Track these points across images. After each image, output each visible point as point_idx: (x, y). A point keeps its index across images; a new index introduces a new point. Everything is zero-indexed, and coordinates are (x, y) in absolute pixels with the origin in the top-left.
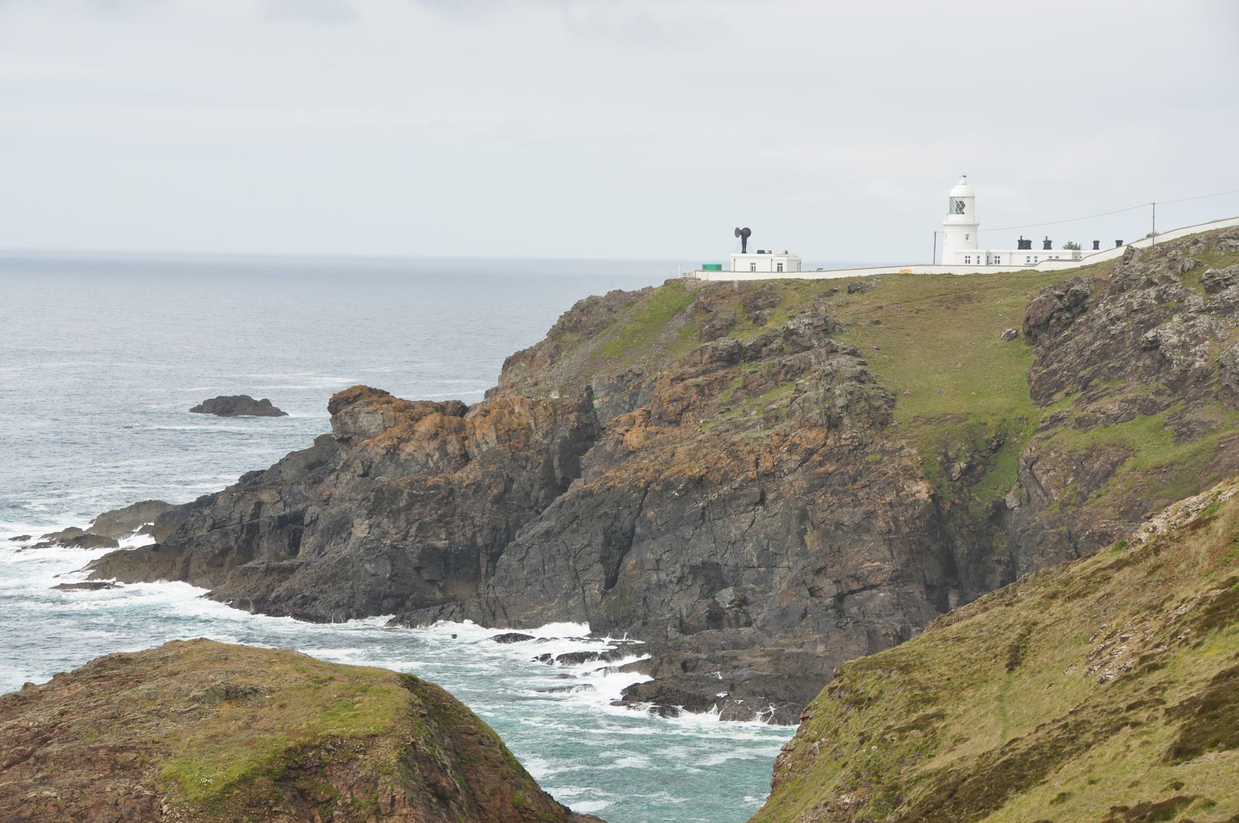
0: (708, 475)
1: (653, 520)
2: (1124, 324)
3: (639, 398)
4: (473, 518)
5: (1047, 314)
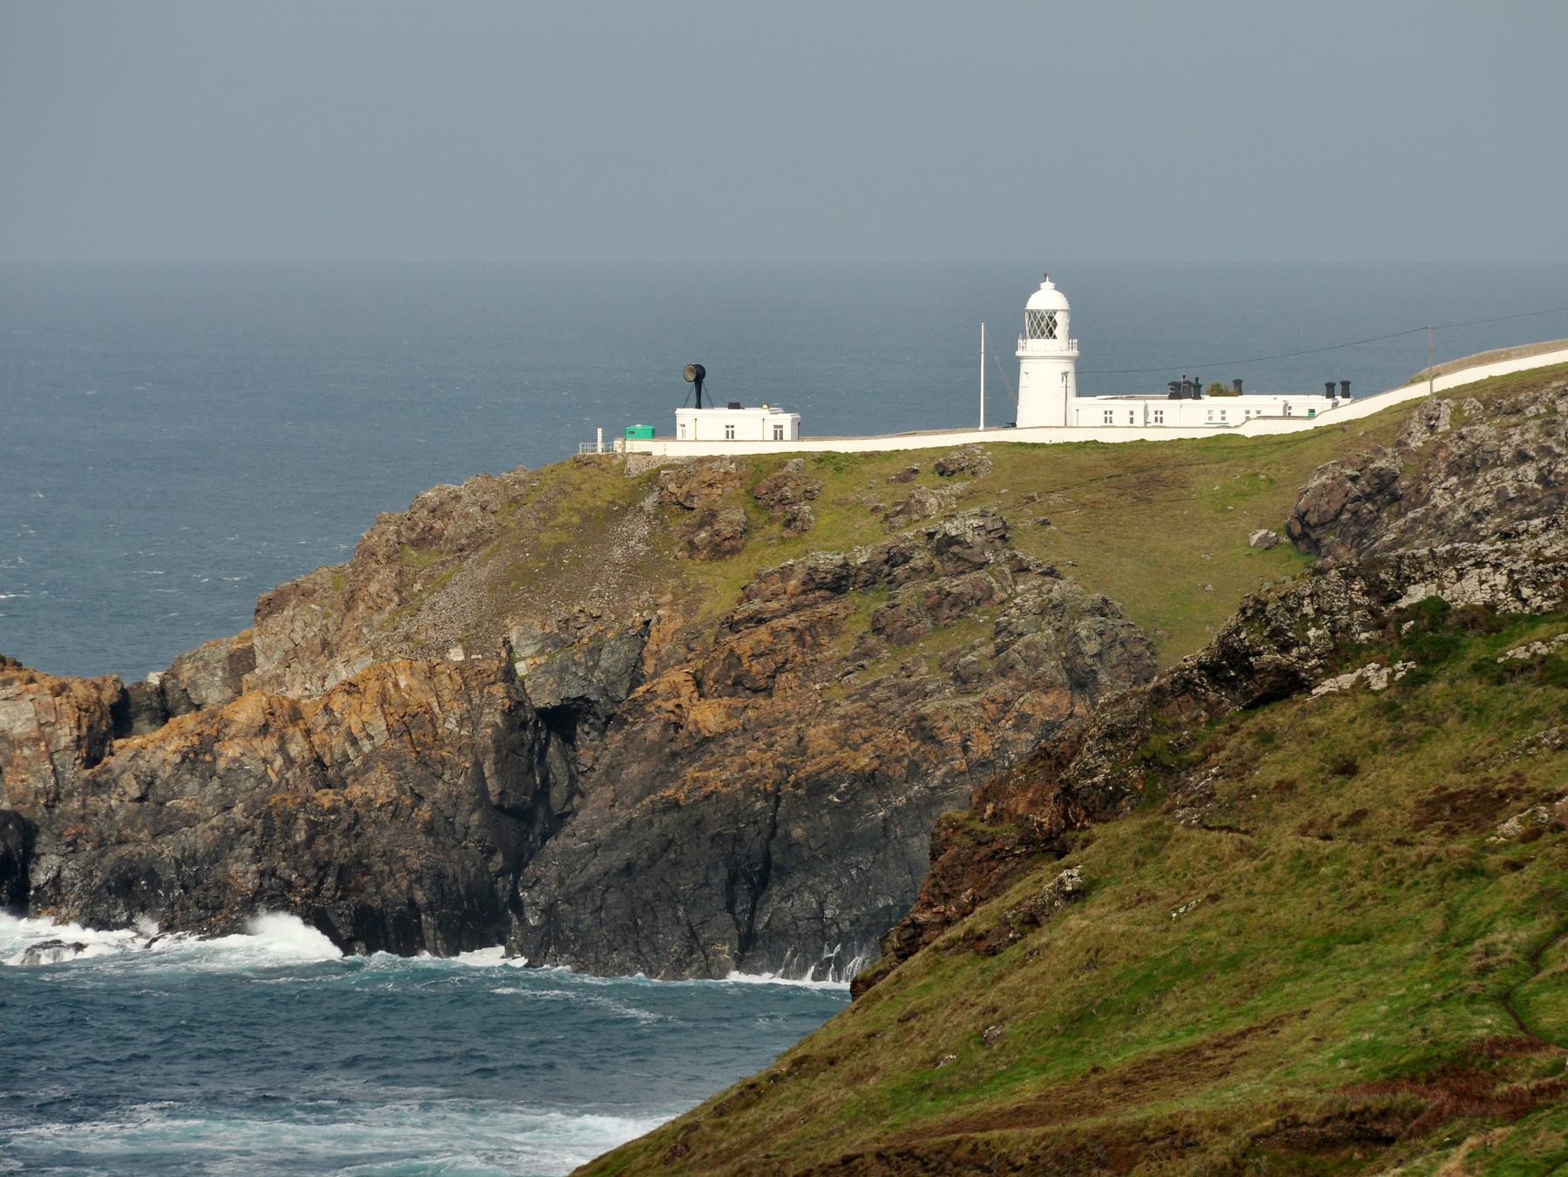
0: (884, 768)
1: (802, 841)
2: (1498, 520)
3: (604, 656)
4: (403, 858)
5: (1336, 506)
